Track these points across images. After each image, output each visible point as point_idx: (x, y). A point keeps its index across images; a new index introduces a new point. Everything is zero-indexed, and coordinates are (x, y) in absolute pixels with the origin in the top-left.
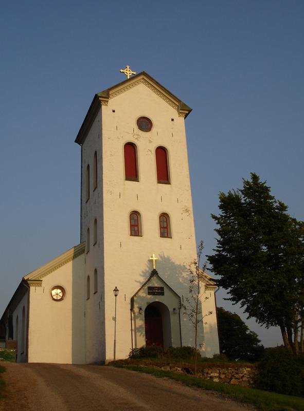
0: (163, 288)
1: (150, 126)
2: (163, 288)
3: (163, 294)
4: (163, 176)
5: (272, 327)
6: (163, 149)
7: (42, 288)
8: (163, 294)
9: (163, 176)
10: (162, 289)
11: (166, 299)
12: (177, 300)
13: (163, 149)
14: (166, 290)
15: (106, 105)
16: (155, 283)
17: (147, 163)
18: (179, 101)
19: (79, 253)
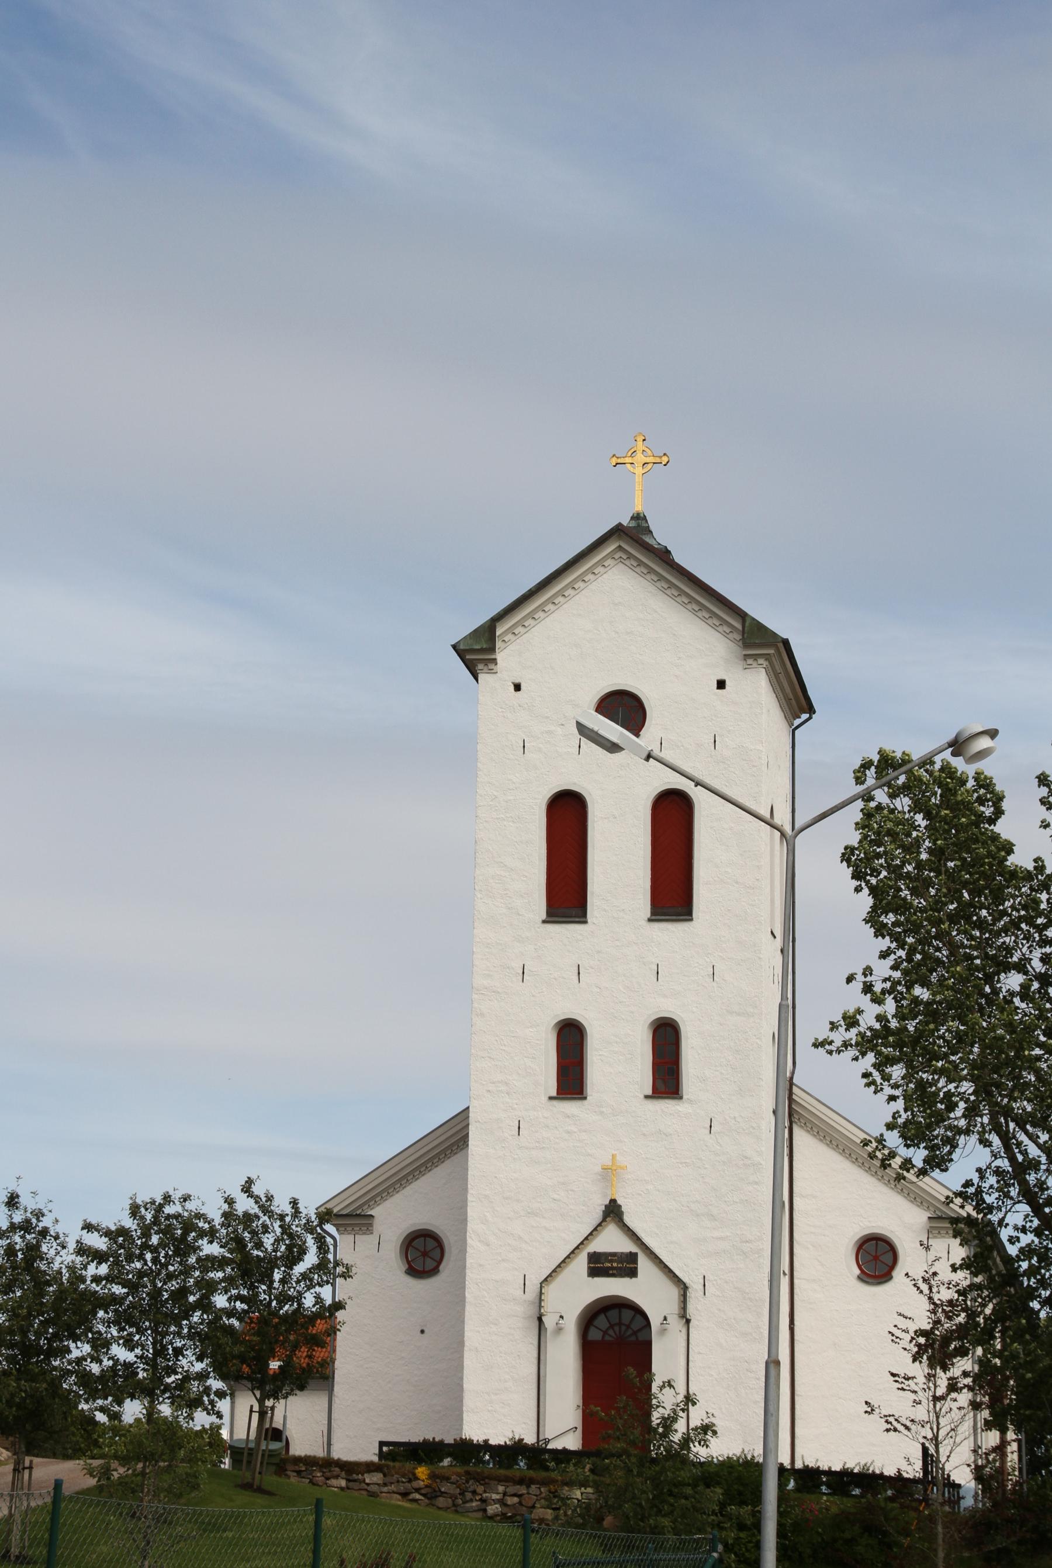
0: (636, 1254)
1: (627, 1315)
2: (636, 1254)
3: (632, 1273)
4: (672, 893)
5: (925, 1219)
6: (413, 1239)
7: (372, 1239)
8: (632, 1273)
9: (672, 893)
10: (632, 1257)
11: (645, 1291)
12: (674, 1292)
13: (413, 1239)
14: (643, 1263)
15: (491, 672)
16: (611, 1241)
17: (619, 856)
18: (742, 615)
19: (444, 1151)
